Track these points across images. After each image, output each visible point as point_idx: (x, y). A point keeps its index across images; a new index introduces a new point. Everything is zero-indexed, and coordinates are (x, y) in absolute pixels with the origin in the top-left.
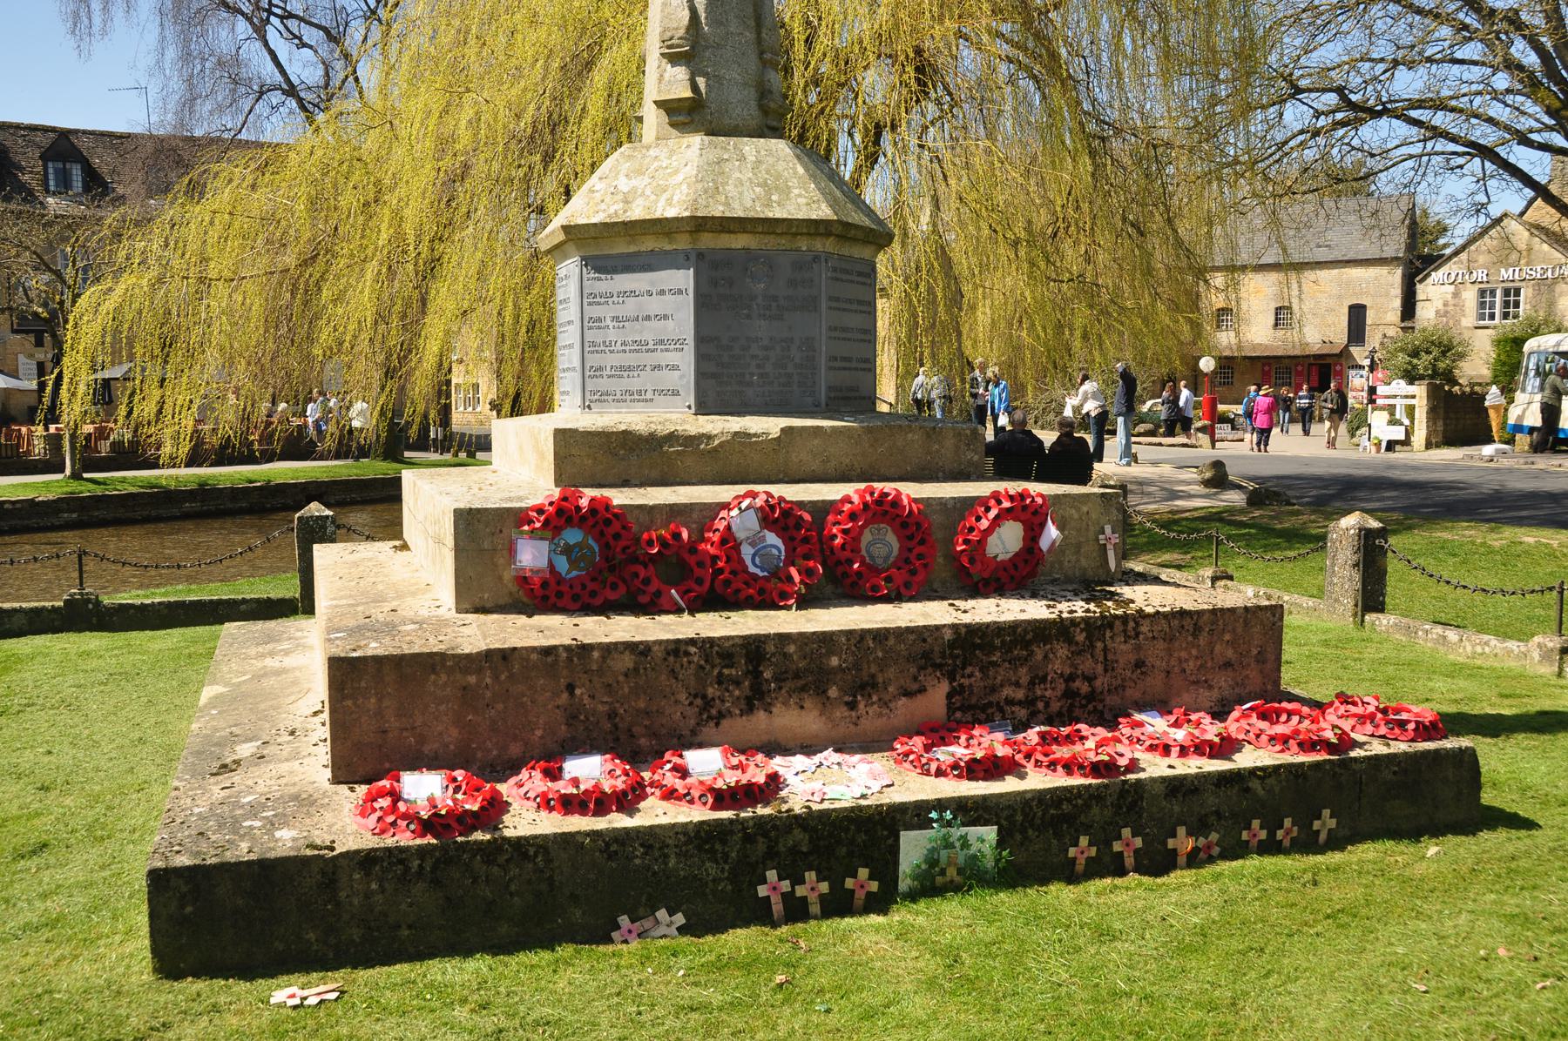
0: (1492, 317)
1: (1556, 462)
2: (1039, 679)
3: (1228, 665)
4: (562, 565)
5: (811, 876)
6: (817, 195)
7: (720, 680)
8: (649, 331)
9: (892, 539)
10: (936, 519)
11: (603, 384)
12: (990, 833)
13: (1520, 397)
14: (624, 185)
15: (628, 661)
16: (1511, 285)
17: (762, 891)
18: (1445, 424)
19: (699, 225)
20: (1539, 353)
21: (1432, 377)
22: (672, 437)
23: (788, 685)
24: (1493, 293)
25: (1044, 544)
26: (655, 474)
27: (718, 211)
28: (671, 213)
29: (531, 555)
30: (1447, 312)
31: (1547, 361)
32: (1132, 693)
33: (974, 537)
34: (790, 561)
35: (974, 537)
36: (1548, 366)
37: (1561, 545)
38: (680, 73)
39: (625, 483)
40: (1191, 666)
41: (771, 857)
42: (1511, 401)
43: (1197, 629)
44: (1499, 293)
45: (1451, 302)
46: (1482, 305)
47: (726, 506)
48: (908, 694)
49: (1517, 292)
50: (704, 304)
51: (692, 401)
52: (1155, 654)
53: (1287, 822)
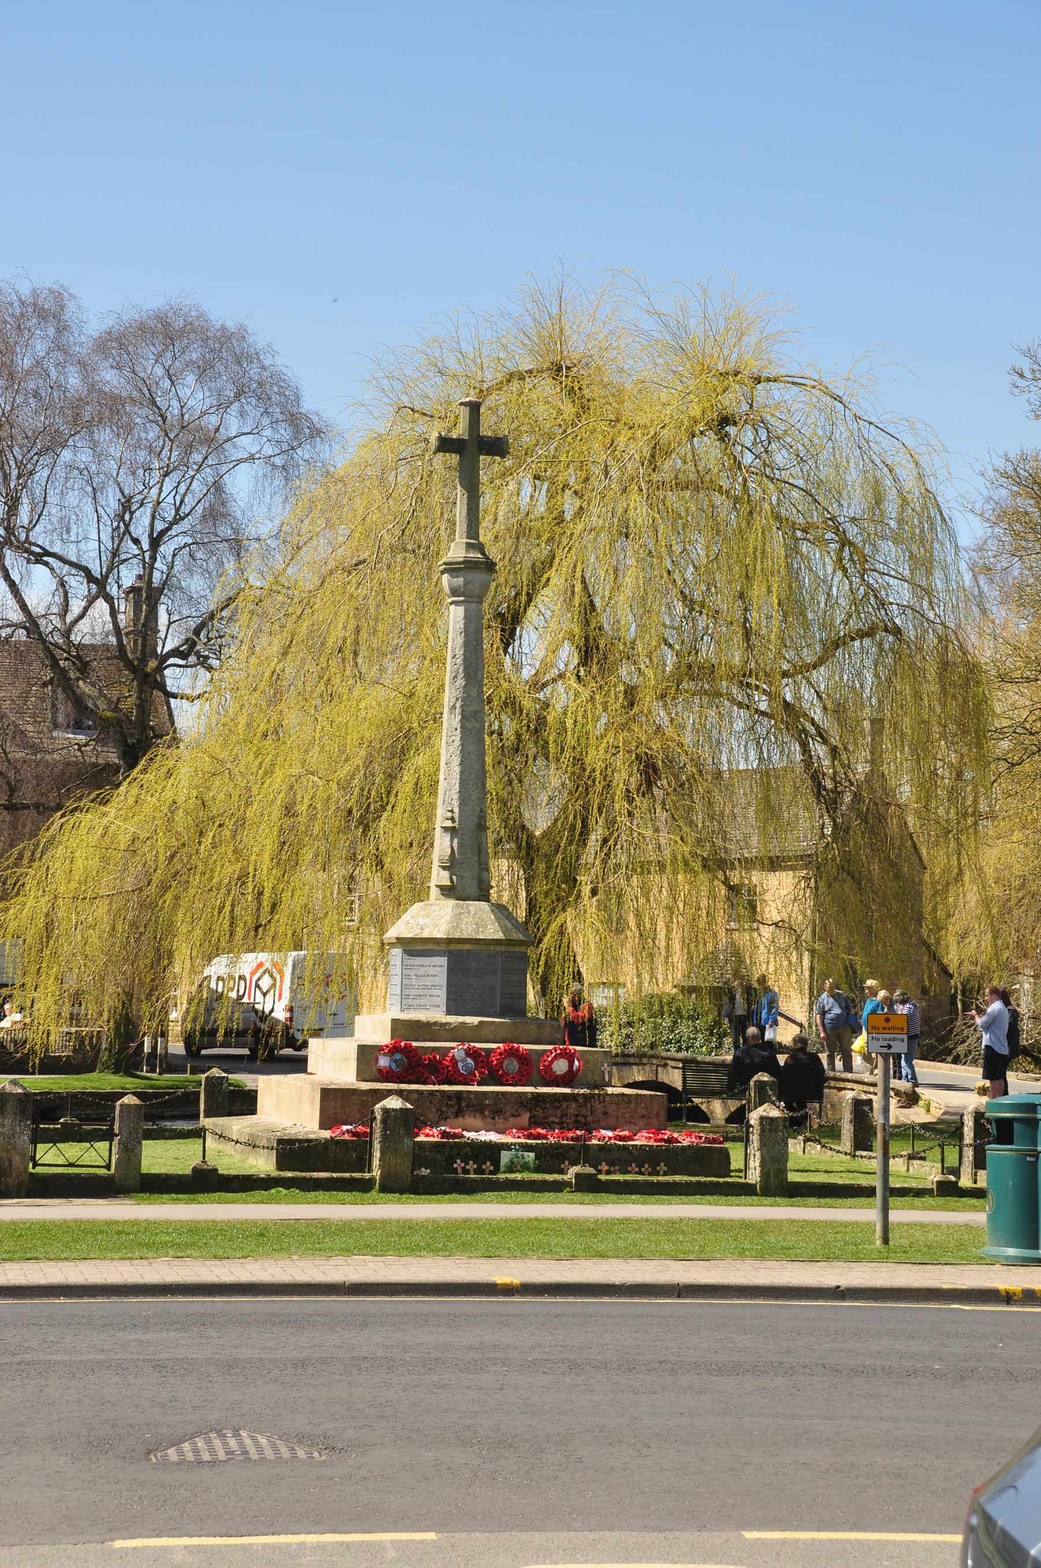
2: (564, 1115)
3: (643, 1116)
4: (394, 1066)
5: (471, 1162)
6: (498, 928)
8: (429, 982)
9: (516, 1063)
10: (534, 1057)
11: (410, 1001)
12: (532, 1155)
14: (421, 921)
17: (455, 1166)
19: (450, 941)
22: (436, 1023)
26: (428, 1037)
27: (457, 935)
28: (439, 936)
29: (384, 1062)
34: (476, 1069)
35: (546, 1063)
38: (446, 874)
39: (417, 1040)
40: (627, 1115)
41: (458, 1155)
43: (629, 1102)
47: (454, 1048)
48: (514, 1116)
50: (451, 971)
51: (445, 1009)
52: (612, 1109)
53: (646, 1166)
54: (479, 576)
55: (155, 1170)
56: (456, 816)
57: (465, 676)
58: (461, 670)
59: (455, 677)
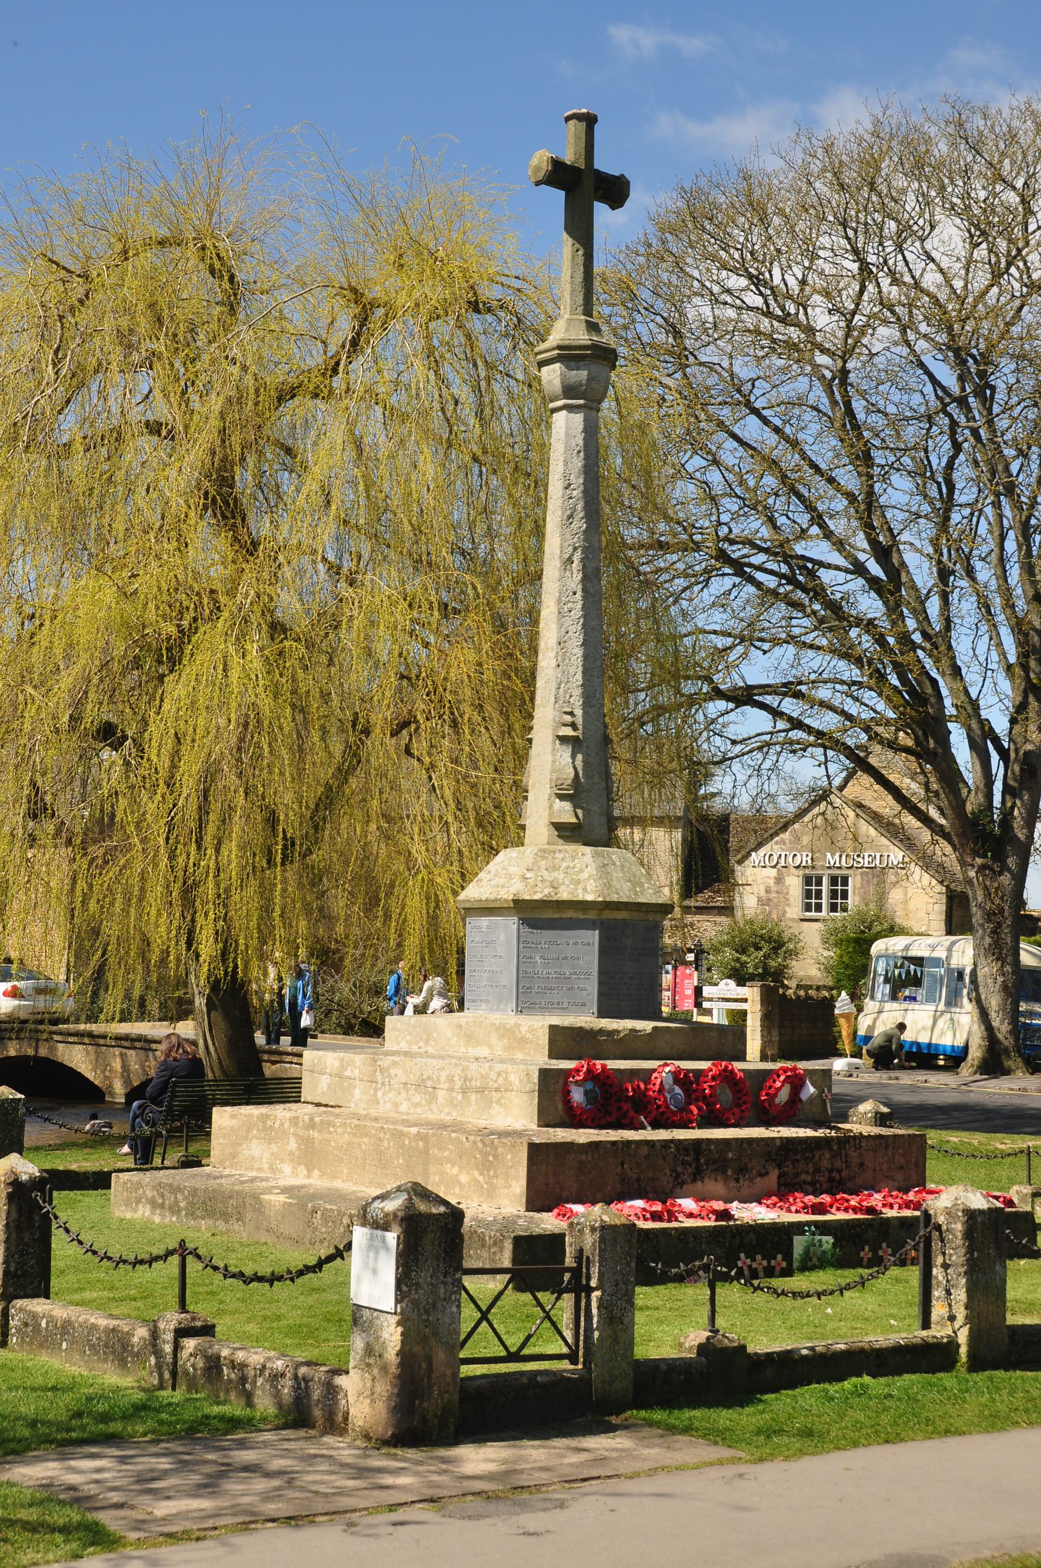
0: (818, 907)
1: (924, 1078)
2: (817, 1170)
3: (901, 1167)
5: (759, 1257)
7: (683, 1163)
12: (831, 1239)
13: (870, 1005)
15: (645, 1150)
16: (838, 872)
18: (780, 1034)
19: (608, 905)
20: (887, 957)
21: (762, 977)
23: (712, 1167)
24: (819, 883)
25: (804, 1096)
27: (615, 898)
28: (590, 898)
30: (769, 900)
31: (896, 967)
32: (859, 1181)
33: (772, 1091)
36: (897, 972)
37: (980, 1143)
38: (567, 806)
40: (885, 1167)
42: (860, 1009)
44: (825, 881)
45: (774, 888)
46: (808, 894)
47: (654, 1071)
48: (761, 1175)
49: (845, 881)
50: (604, 951)
51: (595, 1009)
54: (599, 368)
55: (654, 1354)
56: (579, 721)
57: (585, 516)
58: (580, 507)
59: (571, 516)
